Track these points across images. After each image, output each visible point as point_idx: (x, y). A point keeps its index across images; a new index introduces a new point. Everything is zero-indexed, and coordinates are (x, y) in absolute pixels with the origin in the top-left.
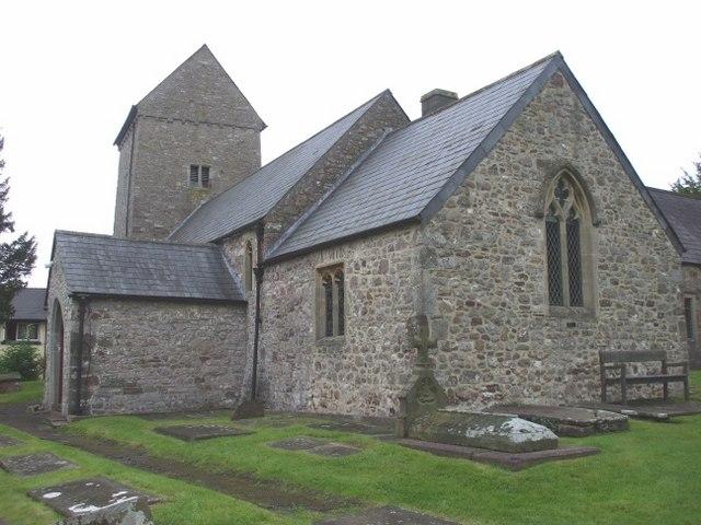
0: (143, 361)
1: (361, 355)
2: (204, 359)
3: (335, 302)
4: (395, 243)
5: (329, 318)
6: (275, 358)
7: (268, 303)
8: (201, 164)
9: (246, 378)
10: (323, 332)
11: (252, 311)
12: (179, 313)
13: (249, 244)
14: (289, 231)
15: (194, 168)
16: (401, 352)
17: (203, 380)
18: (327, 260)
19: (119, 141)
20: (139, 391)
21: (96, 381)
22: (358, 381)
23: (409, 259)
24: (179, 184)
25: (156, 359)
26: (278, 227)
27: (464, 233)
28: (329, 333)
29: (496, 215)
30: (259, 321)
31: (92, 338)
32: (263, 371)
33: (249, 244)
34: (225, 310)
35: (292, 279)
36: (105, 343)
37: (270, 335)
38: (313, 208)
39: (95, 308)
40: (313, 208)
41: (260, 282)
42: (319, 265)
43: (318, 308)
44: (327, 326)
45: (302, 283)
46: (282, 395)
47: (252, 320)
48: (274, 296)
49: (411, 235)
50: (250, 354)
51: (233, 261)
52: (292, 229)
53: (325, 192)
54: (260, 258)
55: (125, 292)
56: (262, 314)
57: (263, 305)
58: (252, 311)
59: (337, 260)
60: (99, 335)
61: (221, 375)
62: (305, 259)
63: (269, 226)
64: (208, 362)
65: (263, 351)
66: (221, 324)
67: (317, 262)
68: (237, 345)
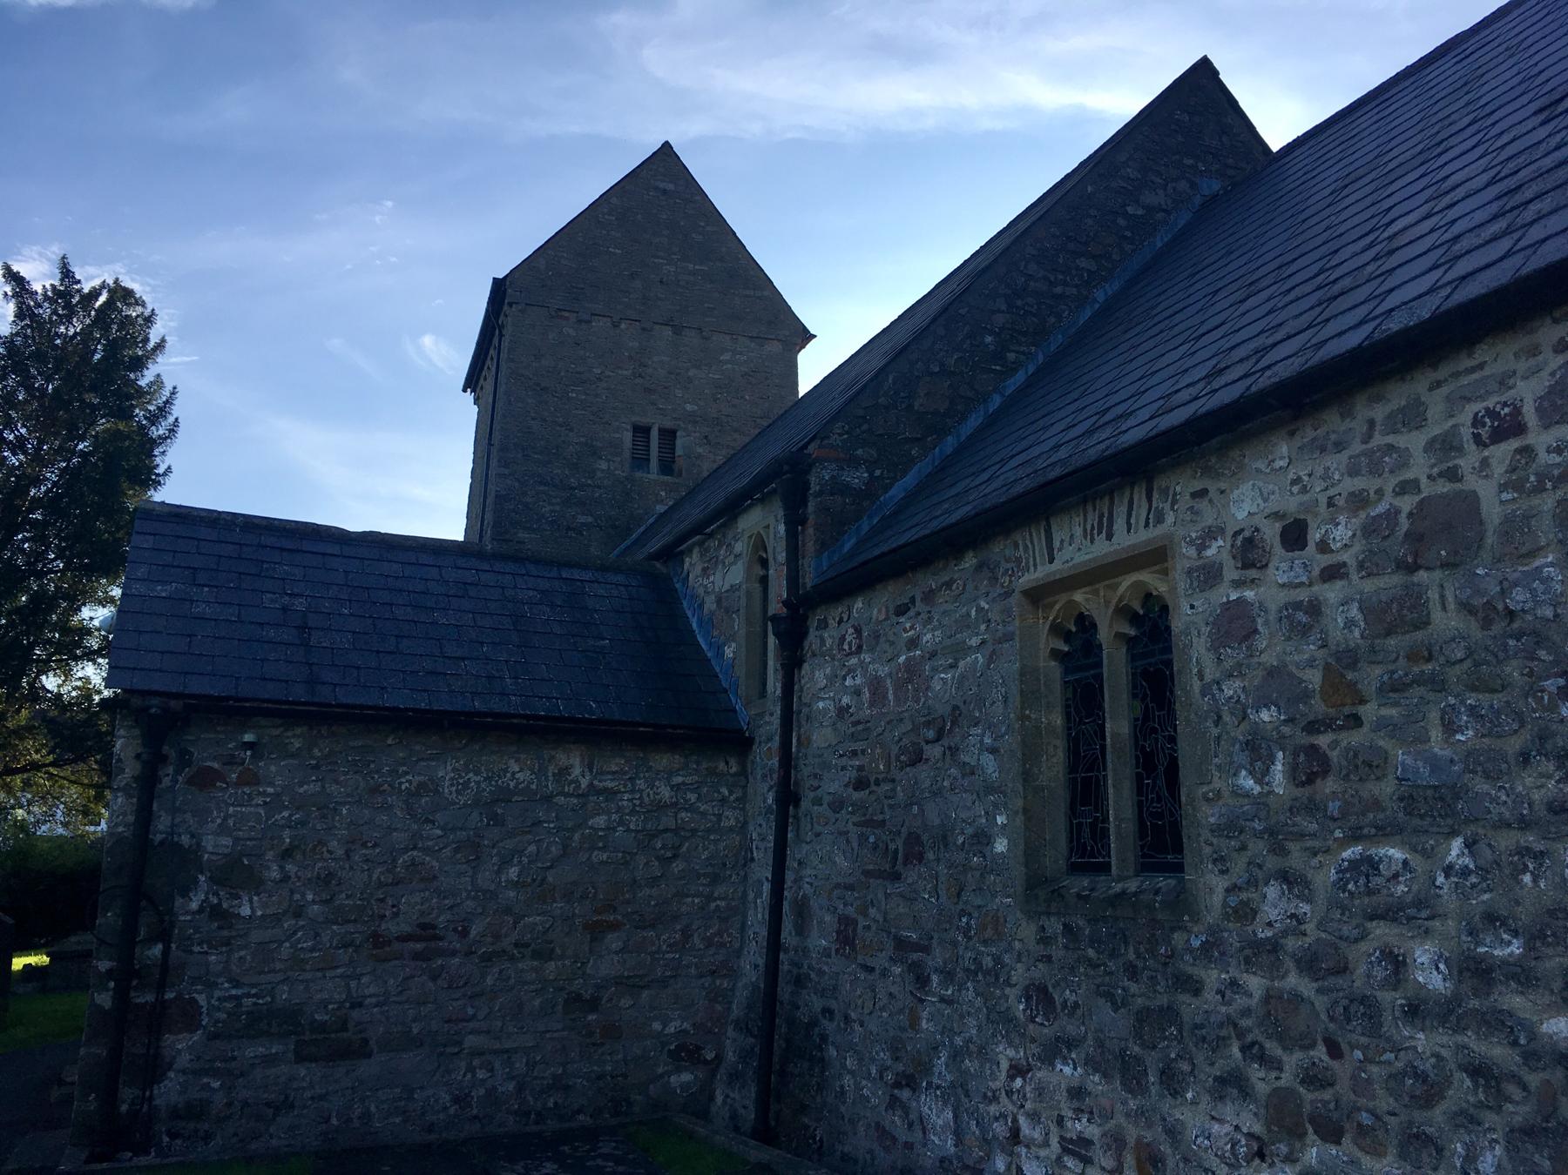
0: (377, 940)
2: (597, 931)
3: (1118, 725)
6: (846, 936)
7: (820, 737)
8: (657, 423)
9: (742, 994)
10: (1055, 856)
11: (766, 756)
12: (518, 770)
13: (760, 544)
14: (897, 491)
15: (642, 431)
17: (593, 1004)
18: (1074, 545)
19: (472, 383)
20: (361, 1051)
21: (190, 1017)
24: (604, 466)
25: (426, 931)
26: (856, 478)
28: (1087, 853)
30: (788, 797)
31: (184, 861)
32: (799, 981)
33: (760, 544)
34: (678, 760)
35: (913, 643)
36: (236, 874)
37: (825, 858)
38: (974, 422)
39: (206, 747)
40: (974, 422)
41: (792, 663)
43: (1030, 753)
44: (1074, 833)
45: (961, 651)
46: (876, 1096)
47: (764, 794)
48: (842, 711)
50: (758, 916)
51: (710, 604)
52: (910, 480)
53: (1012, 370)
54: (793, 580)
55: (617, 717)
56: (805, 770)
57: (805, 742)
58: (766, 756)
60: (215, 845)
61: (663, 983)
62: (970, 561)
63: (819, 478)
64: (613, 941)
65: (802, 910)
66: (660, 807)
68: (715, 879)
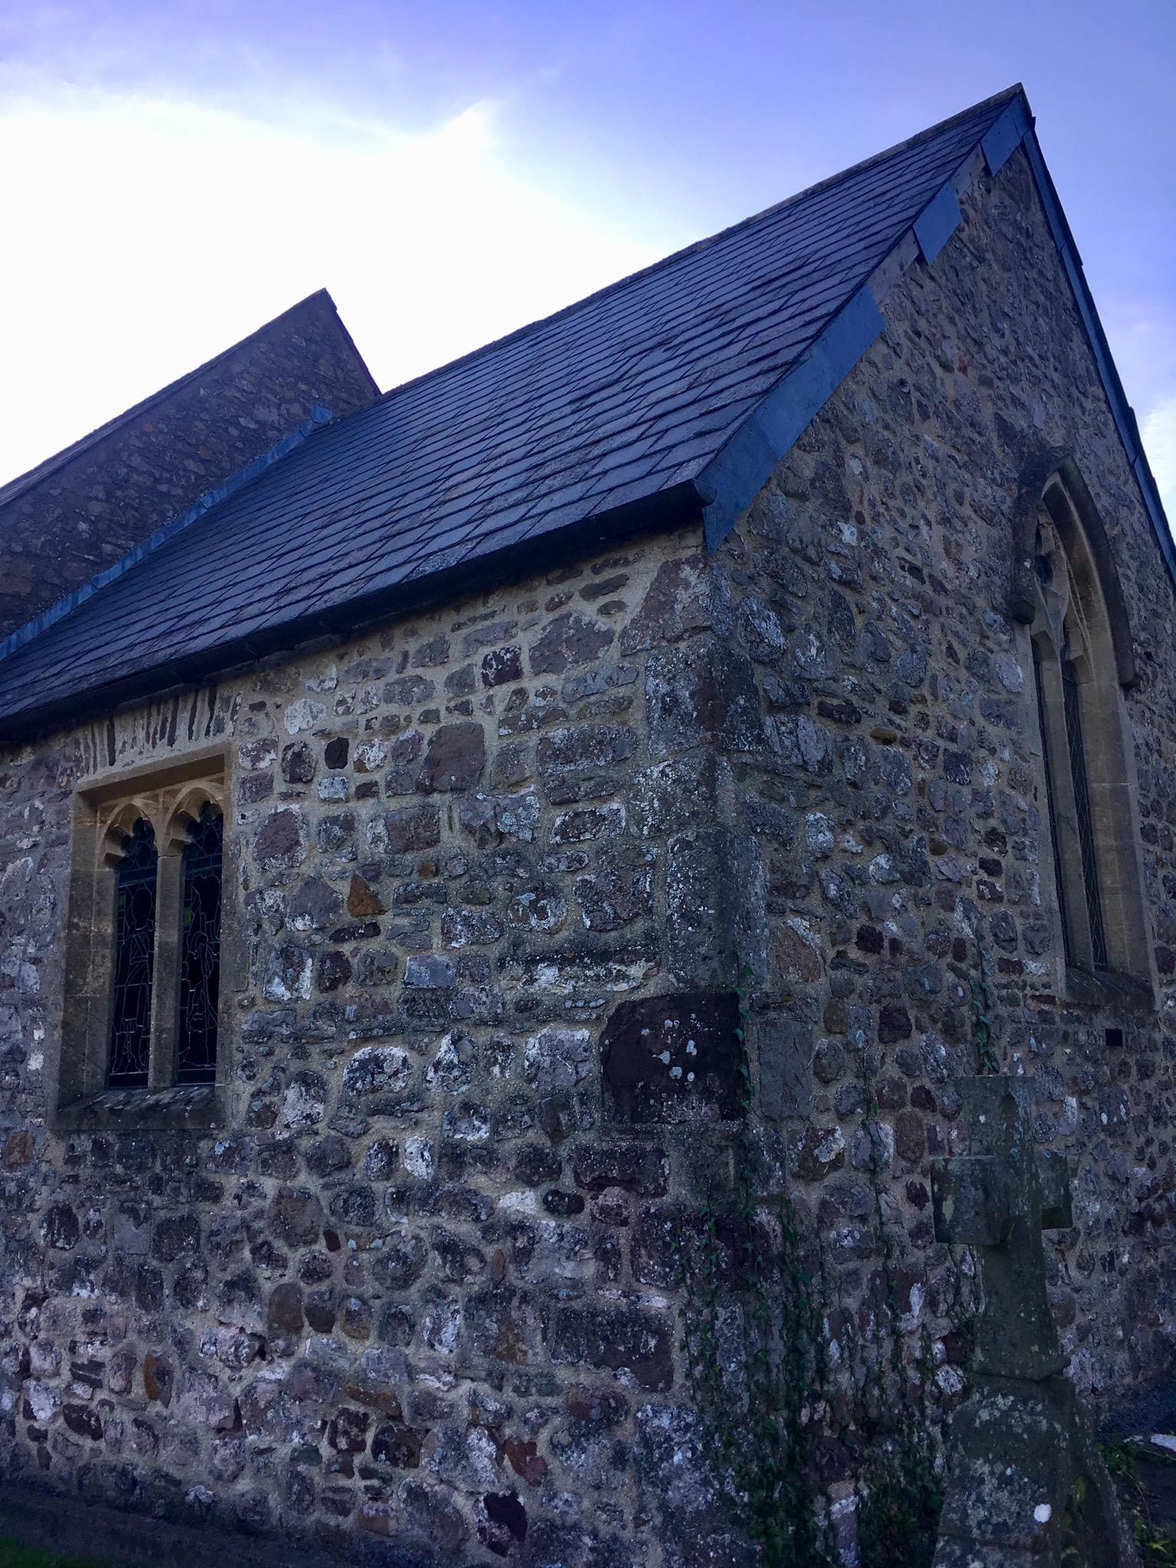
1: (306, 1180)
4: (525, 641)
5: (130, 1002)
16: (567, 1182)
18: (135, 749)
22: (288, 1316)
23: (622, 706)
27: (839, 618)
28: (126, 1068)
29: (915, 571)
42: (85, 781)
49: (634, 595)
53: (106, 562)
59: (187, 746)
62: (27, 758)
67: (79, 766)
